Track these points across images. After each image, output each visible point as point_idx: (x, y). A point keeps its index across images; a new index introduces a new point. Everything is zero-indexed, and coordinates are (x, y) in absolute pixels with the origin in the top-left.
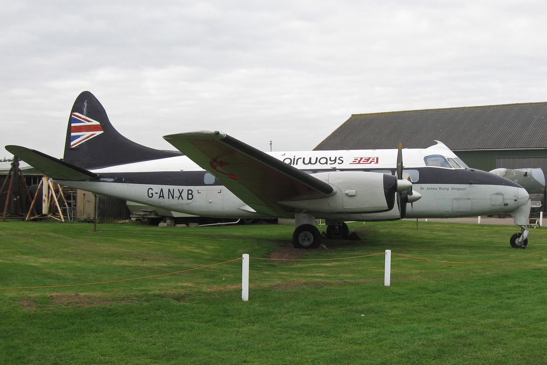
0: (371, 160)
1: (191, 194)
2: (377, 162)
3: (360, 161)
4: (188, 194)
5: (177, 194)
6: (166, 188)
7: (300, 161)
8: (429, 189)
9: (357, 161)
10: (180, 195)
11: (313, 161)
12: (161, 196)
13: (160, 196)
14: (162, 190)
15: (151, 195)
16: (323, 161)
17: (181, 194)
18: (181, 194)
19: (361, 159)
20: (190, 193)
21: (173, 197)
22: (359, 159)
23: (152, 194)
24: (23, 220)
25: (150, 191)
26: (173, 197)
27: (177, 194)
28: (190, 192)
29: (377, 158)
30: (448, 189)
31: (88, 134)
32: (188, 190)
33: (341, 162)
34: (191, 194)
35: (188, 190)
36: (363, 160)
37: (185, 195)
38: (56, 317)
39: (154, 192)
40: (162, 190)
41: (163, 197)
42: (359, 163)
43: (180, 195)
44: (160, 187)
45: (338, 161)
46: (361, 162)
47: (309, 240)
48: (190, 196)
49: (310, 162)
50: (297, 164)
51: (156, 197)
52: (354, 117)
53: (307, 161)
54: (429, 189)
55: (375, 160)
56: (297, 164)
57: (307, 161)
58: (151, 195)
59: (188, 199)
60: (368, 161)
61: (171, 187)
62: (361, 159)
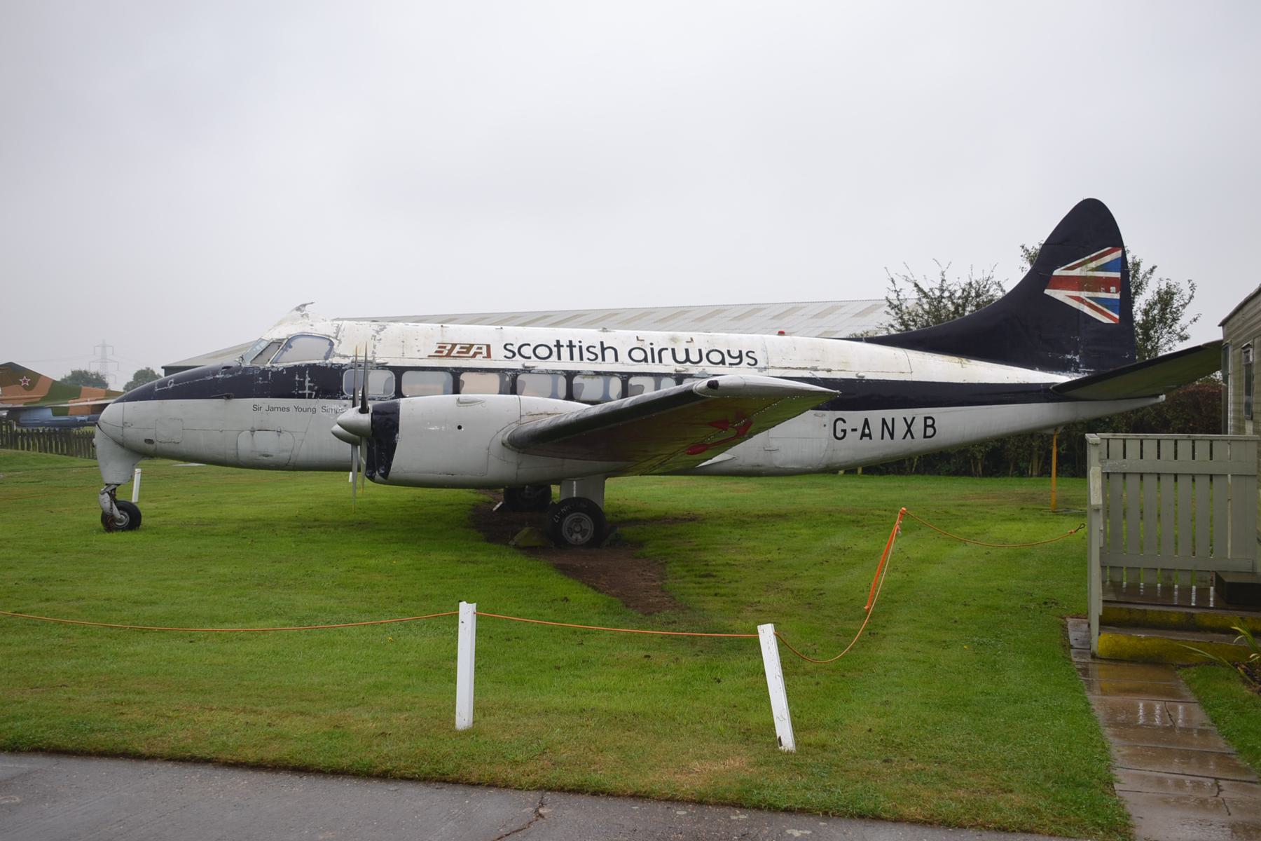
1: (932, 426)
2: (489, 356)
3: (451, 351)
4: (926, 426)
5: (901, 428)
6: (876, 416)
7: (667, 356)
8: (273, 409)
10: (909, 430)
11: (694, 357)
13: (863, 435)
14: (866, 422)
15: (840, 434)
16: (716, 357)
17: (909, 427)
18: (909, 427)
19: (454, 345)
20: (929, 424)
21: (892, 436)
22: (449, 347)
24: (507, 544)
25: (840, 425)
26: (892, 436)
27: (901, 428)
28: (929, 422)
29: (488, 347)
30: (314, 410)
32: (926, 418)
34: (932, 426)
35: (926, 418)
36: (457, 348)
37: (918, 427)
38: (980, 821)
39: (848, 427)
40: (866, 422)
41: (870, 436)
42: (448, 355)
43: (909, 430)
45: (746, 360)
47: (583, 532)
49: (688, 360)
50: (660, 361)
51: (853, 438)
53: (681, 356)
54: (273, 409)
55: (485, 348)
57: (681, 356)
58: (840, 434)
59: (925, 436)
60: (468, 352)
61: (888, 414)
62: (454, 345)
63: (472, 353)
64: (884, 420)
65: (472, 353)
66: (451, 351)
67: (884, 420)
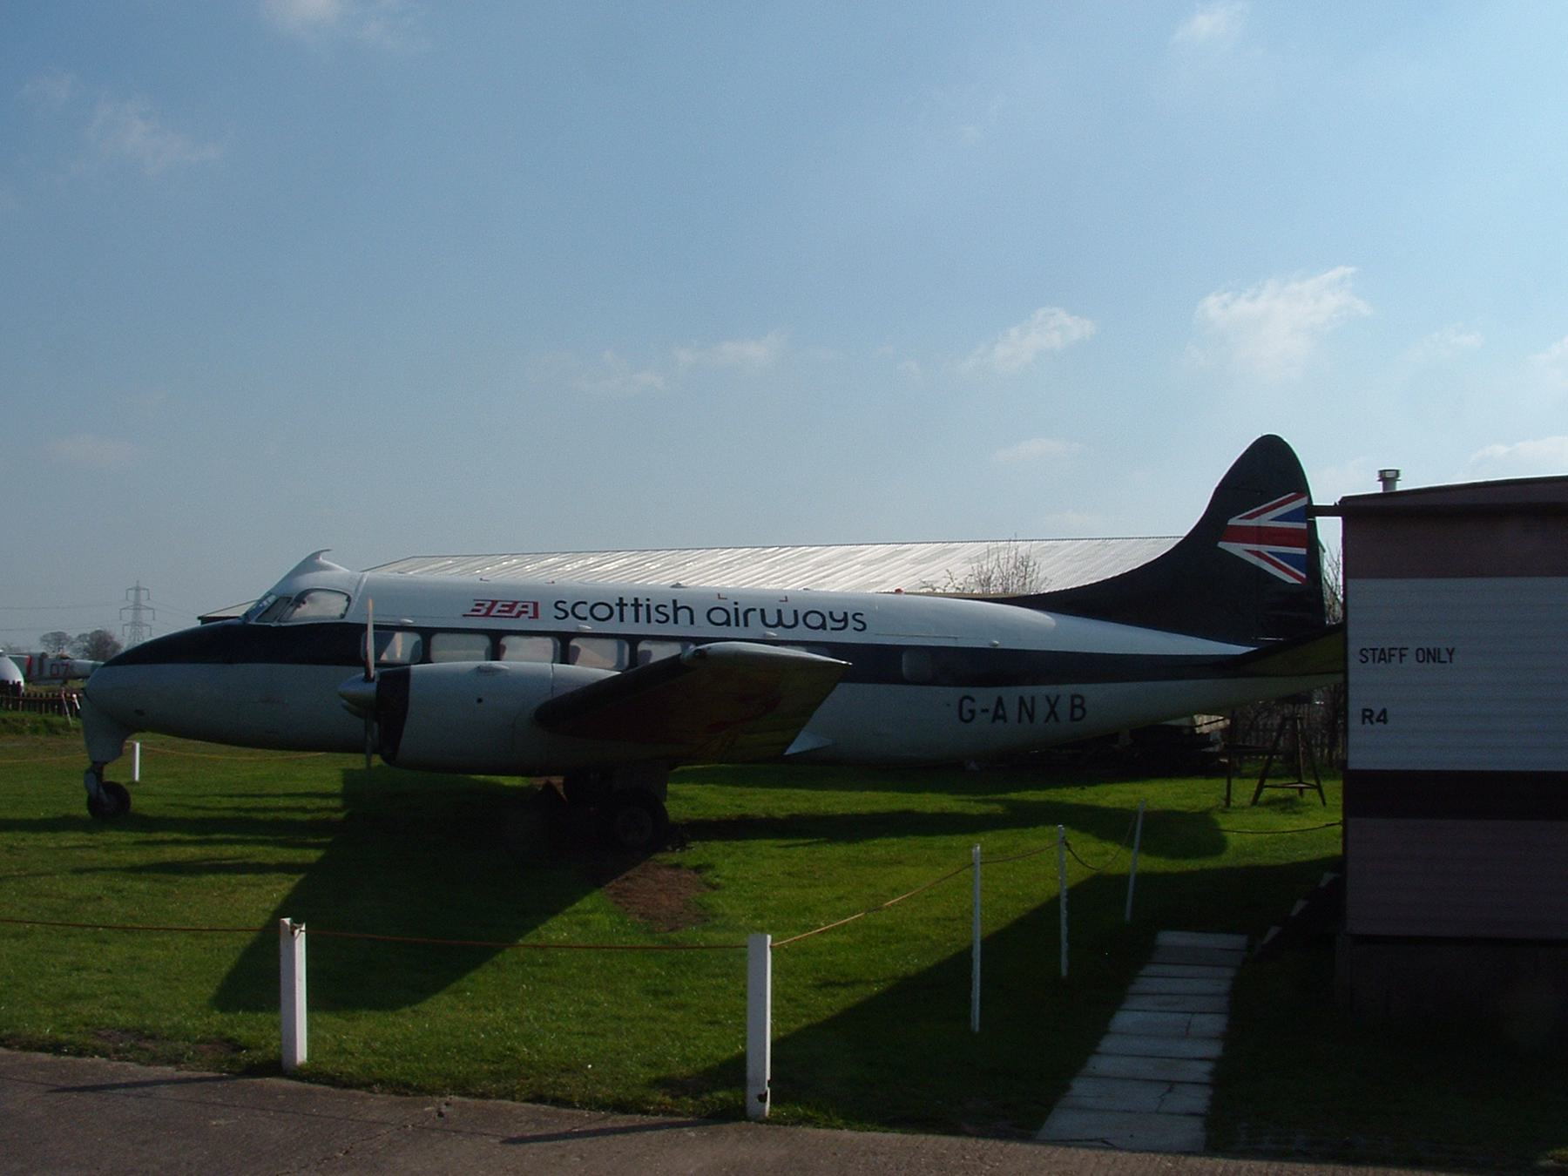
0: (518, 608)
1: (1081, 706)
2: (536, 616)
3: (490, 610)
4: (1073, 706)
6: (1011, 694)
9: (484, 611)
12: (999, 715)
13: (996, 717)
14: (1000, 702)
15: (967, 716)
17: (1053, 707)
18: (1053, 707)
19: (494, 603)
22: (488, 604)
23: (972, 711)
27: (1042, 710)
28: (1078, 701)
29: (536, 604)
31: (1265, 521)
33: (860, 626)
36: (498, 607)
39: (977, 707)
40: (1000, 702)
41: (1004, 718)
42: (487, 615)
44: (995, 692)
46: (494, 612)
48: (1078, 712)
49: (780, 623)
50: (746, 625)
52: (1263, 438)
53: (772, 618)
55: (531, 609)
56: (746, 625)
58: (967, 716)
59: (1073, 719)
61: (1027, 691)
62: (494, 603)
63: (514, 613)
64: (1021, 698)
65: (514, 613)
66: (490, 610)
67: (1021, 698)
